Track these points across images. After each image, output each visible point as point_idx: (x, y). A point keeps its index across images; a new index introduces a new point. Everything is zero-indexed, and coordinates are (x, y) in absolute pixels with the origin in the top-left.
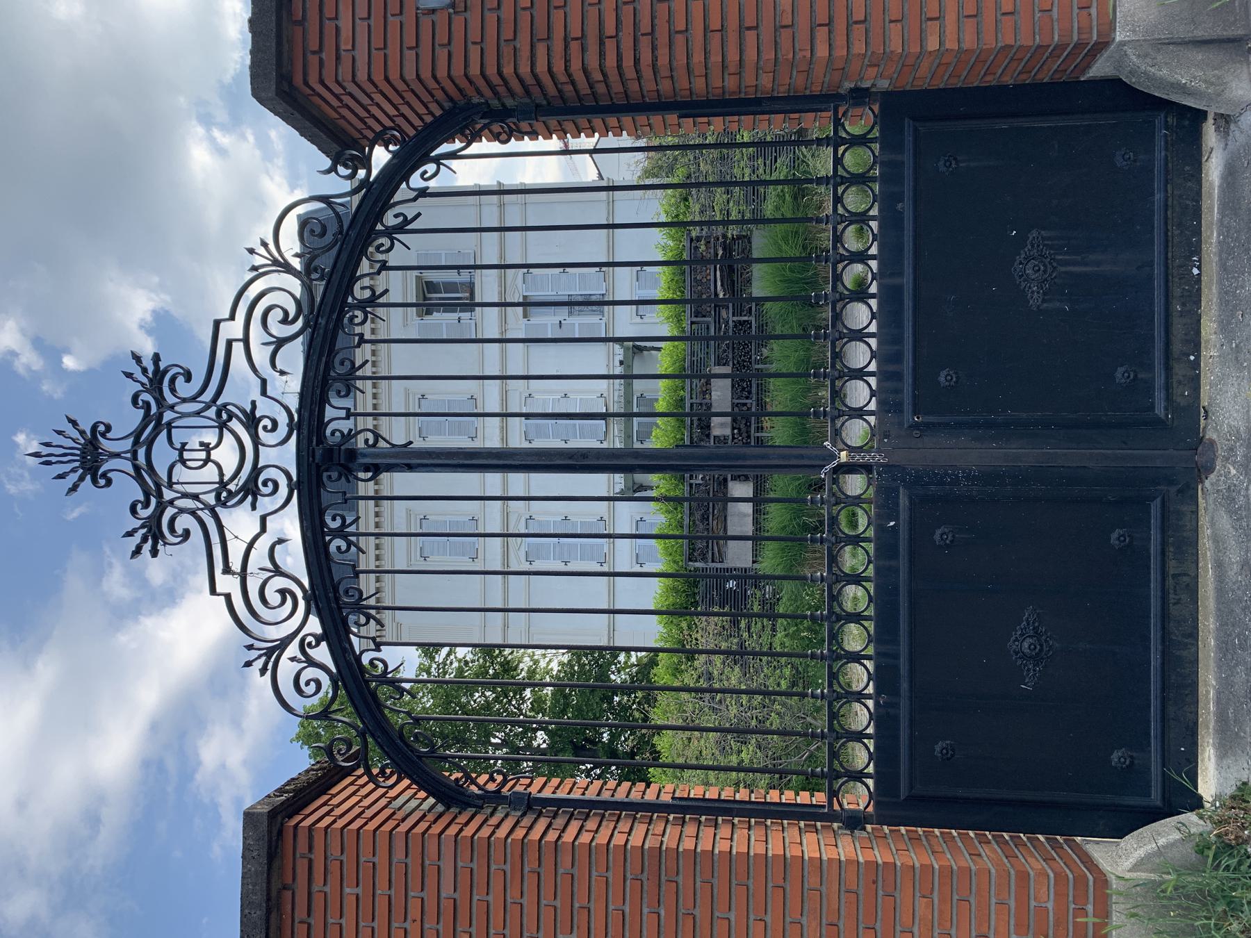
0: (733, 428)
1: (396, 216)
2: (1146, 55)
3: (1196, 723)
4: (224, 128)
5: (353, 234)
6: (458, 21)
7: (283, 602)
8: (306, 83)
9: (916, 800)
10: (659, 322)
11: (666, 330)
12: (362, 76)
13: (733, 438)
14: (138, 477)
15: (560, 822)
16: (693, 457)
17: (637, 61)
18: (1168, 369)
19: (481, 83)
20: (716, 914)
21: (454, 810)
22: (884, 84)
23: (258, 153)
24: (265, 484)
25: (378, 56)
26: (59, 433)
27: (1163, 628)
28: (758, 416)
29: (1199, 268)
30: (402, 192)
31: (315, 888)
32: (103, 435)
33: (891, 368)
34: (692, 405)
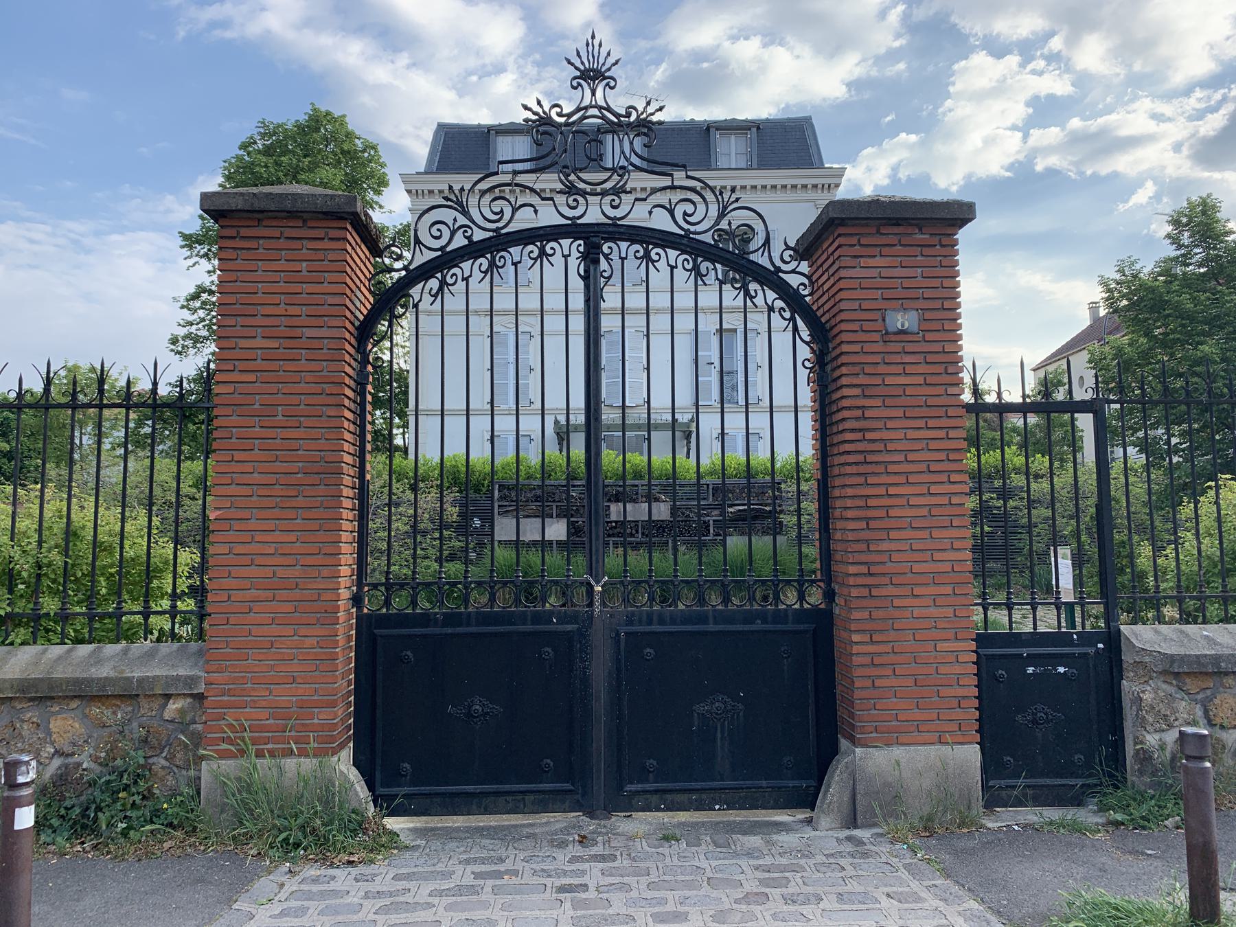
0: (616, 522)
1: (755, 291)
2: (847, 767)
3: (430, 815)
4: (906, 17)
5: (743, 262)
6: (876, 337)
7: (496, 214)
8: (839, 235)
9: (374, 639)
10: (710, 456)
11: (705, 462)
12: (843, 273)
13: (608, 522)
14: (578, 110)
15: (352, 406)
16: (597, 492)
17: (848, 453)
18: (656, 791)
19: (838, 351)
20: (300, 511)
21: (355, 333)
22: (837, 611)
23: (883, 51)
24: (575, 200)
25: (855, 284)
26: (609, 54)
27: (490, 793)
28: (624, 545)
29: (719, 809)
30: (771, 295)
31: (305, 242)
32: (608, 84)
33: (655, 618)
34: (637, 486)
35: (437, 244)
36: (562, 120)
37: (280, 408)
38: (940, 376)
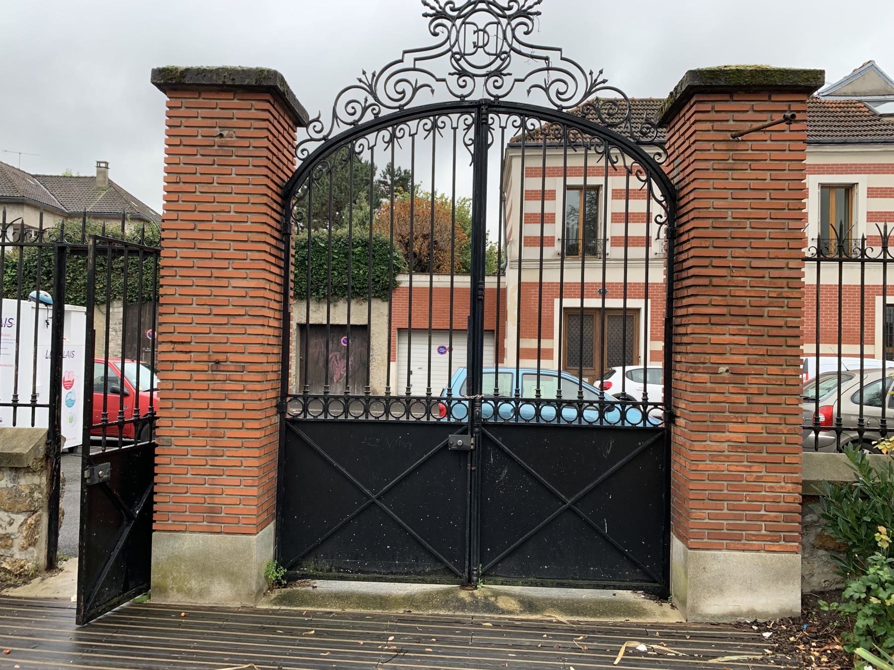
30: (629, 161)
35: (351, 119)
36: (455, 14)
37: (725, 503)
38: (706, 230)
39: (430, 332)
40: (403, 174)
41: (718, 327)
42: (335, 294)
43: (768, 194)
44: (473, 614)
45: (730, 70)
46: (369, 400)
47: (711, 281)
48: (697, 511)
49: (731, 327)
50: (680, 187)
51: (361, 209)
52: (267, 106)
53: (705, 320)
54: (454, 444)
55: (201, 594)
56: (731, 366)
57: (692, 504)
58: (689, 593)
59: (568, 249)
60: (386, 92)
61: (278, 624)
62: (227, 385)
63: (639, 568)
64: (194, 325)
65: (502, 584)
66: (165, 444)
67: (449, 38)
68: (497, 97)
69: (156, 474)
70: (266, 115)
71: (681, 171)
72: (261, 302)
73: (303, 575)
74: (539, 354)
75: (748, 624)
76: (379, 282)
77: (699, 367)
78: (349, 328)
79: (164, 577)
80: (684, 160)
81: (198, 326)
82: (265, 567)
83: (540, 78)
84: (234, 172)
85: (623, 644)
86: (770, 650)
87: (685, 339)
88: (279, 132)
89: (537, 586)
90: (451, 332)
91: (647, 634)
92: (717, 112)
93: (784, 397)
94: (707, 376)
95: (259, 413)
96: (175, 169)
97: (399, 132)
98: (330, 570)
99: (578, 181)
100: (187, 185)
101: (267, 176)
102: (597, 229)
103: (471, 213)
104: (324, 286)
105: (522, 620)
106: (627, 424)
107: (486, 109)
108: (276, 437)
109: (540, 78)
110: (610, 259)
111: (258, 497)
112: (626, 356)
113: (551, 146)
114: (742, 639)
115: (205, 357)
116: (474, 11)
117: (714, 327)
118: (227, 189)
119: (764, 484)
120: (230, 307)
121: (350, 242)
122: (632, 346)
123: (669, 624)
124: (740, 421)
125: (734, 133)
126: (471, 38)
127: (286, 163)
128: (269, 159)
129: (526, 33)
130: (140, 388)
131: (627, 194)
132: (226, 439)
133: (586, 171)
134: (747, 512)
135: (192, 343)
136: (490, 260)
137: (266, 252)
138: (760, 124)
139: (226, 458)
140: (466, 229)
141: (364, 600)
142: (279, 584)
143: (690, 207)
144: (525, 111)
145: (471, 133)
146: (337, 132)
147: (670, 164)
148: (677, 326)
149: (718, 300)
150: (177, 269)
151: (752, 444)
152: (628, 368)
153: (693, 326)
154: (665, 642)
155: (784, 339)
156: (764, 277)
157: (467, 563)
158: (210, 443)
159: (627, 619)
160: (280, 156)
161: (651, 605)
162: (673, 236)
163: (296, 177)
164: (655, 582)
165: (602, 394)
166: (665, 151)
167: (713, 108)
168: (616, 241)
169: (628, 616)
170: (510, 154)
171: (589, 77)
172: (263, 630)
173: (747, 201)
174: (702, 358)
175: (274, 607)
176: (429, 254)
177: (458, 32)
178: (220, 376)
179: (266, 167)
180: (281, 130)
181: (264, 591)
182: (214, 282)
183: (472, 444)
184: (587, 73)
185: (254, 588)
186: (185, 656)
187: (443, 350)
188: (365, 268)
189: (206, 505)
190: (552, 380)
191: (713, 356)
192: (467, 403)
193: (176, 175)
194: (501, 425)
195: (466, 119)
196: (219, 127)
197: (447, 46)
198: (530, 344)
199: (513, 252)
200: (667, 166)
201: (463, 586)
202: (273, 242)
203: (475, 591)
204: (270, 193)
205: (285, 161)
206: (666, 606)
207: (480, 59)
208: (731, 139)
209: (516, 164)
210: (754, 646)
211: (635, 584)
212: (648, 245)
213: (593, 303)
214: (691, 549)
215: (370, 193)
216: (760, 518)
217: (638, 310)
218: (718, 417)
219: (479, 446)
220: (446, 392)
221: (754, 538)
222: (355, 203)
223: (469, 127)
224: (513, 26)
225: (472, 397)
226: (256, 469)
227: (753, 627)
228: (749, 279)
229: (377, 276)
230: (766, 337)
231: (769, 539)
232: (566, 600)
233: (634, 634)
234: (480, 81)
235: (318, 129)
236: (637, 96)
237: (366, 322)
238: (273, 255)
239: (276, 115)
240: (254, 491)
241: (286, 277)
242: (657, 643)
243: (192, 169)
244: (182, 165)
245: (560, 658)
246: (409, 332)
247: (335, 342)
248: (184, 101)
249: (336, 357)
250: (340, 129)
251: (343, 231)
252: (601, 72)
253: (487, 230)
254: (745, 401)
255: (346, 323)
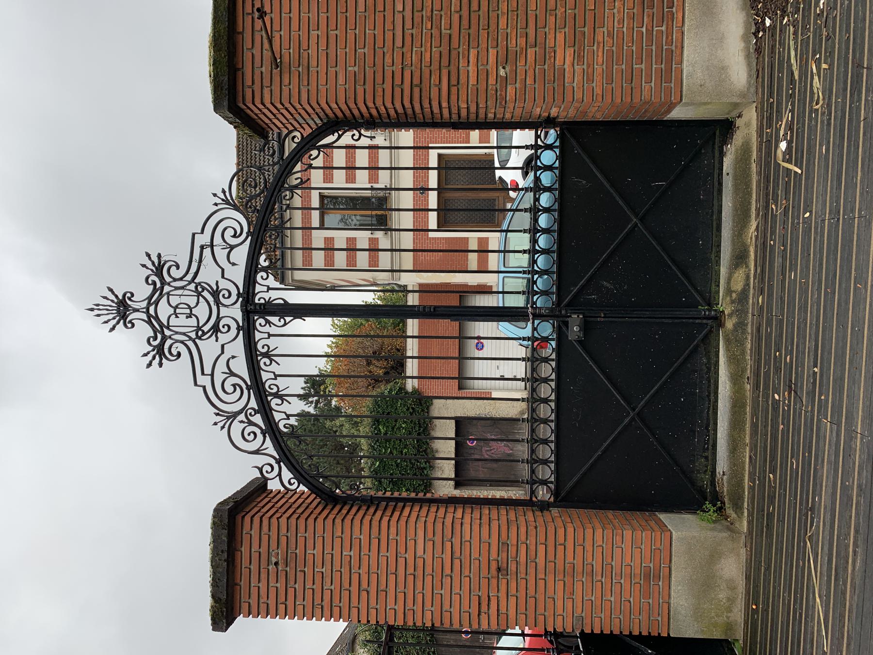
30: (298, 167)
35: (260, 437)
36: (159, 336)
37: (635, 66)
38: (367, 90)
39: (462, 358)
40: (308, 385)
41: (461, 78)
42: (425, 451)
43: (332, 32)
44: (750, 315)
45: (213, 71)
46: (534, 420)
47: (416, 86)
48: (643, 94)
49: (461, 65)
50: (325, 117)
51: (342, 425)
52: (247, 519)
53: (454, 90)
54: (578, 334)
55: (733, 588)
56: (499, 64)
57: (636, 100)
58: (725, 100)
59: (381, 224)
60: (234, 402)
61: (763, 511)
62: (521, 560)
63: (700, 150)
64: (461, 593)
65: (718, 286)
66: (581, 622)
67: (182, 342)
68: (239, 295)
69: (611, 631)
70: (257, 519)
71: (310, 116)
72: (439, 526)
73: (711, 485)
74: (483, 251)
75: (757, 41)
76: (413, 408)
77: (501, 95)
78: (459, 439)
79: (715, 625)
80: (299, 114)
81: (462, 588)
82: (704, 524)
83: (221, 254)
84: (312, 552)
85: (779, 164)
86: (784, 19)
87: (473, 109)
88: (273, 506)
89: (720, 251)
90: (462, 338)
91: (769, 141)
92: (253, 83)
93: (529, 12)
94: (509, 87)
95: (548, 529)
96: (309, 609)
97: (272, 389)
98: (706, 458)
99: (315, 215)
100: (324, 598)
101: (315, 519)
102: (361, 197)
103: (346, 319)
104: (418, 462)
105: (756, 265)
106: (557, 164)
107: (251, 305)
108: (573, 511)
109: (221, 254)
110: (391, 184)
111: (634, 530)
112: (485, 166)
113: (282, 243)
114: (773, 47)
115: (494, 582)
116: (157, 318)
117: (461, 82)
118: (328, 558)
119: (616, 29)
120: (444, 556)
121: (375, 437)
122: (475, 161)
123: (757, 119)
124: (553, 54)
125: (273, 66)
126: (182, 320)
127: (268, 499)
128: (299, 516)
129: (178, 267)
130: (521, 646)
131: (328, 168)
132: (575, 562)
133: (307, 209)
134: (644, 45)
135: (480, 594)
136: (392, 300)
137: (389, 520)
138: (266, 41)
139: (594, 562)
140: (362, 324)
141: (736, 424)
142: (720, 510)
143: (344, 107)
144: (252, 269)
145: (274, 319)
146: (272, 451)
147: (303, 127)
148: (459, 117)
149: (435, 79)
150: (407, 608)
151: (576, 41)
152: (497, 165)
153: (460, 102)
154: (777, 123)
155: (472, 14)
156: (412, 34)
157: (697, 321)
158: (580, 578)
159: (753, 161)
160: (296, 505)
161: (738, 138)
162: (372, 123)
163: (316, 490)
164: (715, 134)
165: (522, 189)
166: (290, 132)
167: (249, 87)
168: (373, 179)
169: (750, 161)
170: (290, 282)
171: (220, 207)
172: (769, 527)
173: (338, 53)
174: (491, 92)
175: (746, 514)
176: (386, 360)
177: (177, 333)
178: (512, 567)
179: (306, 519)
180: (270, 505)
181: (729, 524)
182: (420, 572)
183: (578, 316)
184: (216, 208)
185: (725, 535)
186: (798, 605)
187: (480, 345)
188: (400, 422)
189: (642, 582)
190: (509, 238)
191: (490, 83)
192: (536, 322)
193: (315, 608)
194: (558, 288)
195: (260, 324)
196: (268, 565)
197: (190, 344)
198: (473, 260)
199: (383, 278)
200: (304, 130)
201: (721, 324)
202: (379, 513)
203: (726, 313)
204: (331, 516)
205: (300, 501)
206: (739, 122)
207: (202, 311)
208: (279, 69)
209: (300, 276)
210: (780, 34)
211: (717, 154)
212: (378, 147)
213: (433, 199)
214: (681, 100)
215: (326, 417)
216: (650, 32)
217: (440, 156)
218: (549, 76)
219: (579, 310)
220: (525, 343)
221: (670, 38)
222: (337, 431)
223: (268, 322)
224: (171, 280)
225: (531, 317)
226: (605, 532)
227: (760, 36)
228: (415, 49)
229: (408, 409)
230: (471, 31)
231: (670, 23)
232: (734, 222)
233: (768, 154)
234: (224, 311)
235: (269, 469)
236: (234, 159)
237: (453, 422)
238: (393, 513)
239: (256, 509)
240: (628, 534)
241: (414, 501)
242: (778, 131)
243: (309, 593)
244: (305, 603)
245: (795, 228)
246: (462, 379)
247: (473, 452)
248: (243, 600)
249: (488, 451)
250: (269, 447)
251: (364, 443)
252: (215, 195)
253: (362, 303)
254: (533, 49)
255: (453, 442)
